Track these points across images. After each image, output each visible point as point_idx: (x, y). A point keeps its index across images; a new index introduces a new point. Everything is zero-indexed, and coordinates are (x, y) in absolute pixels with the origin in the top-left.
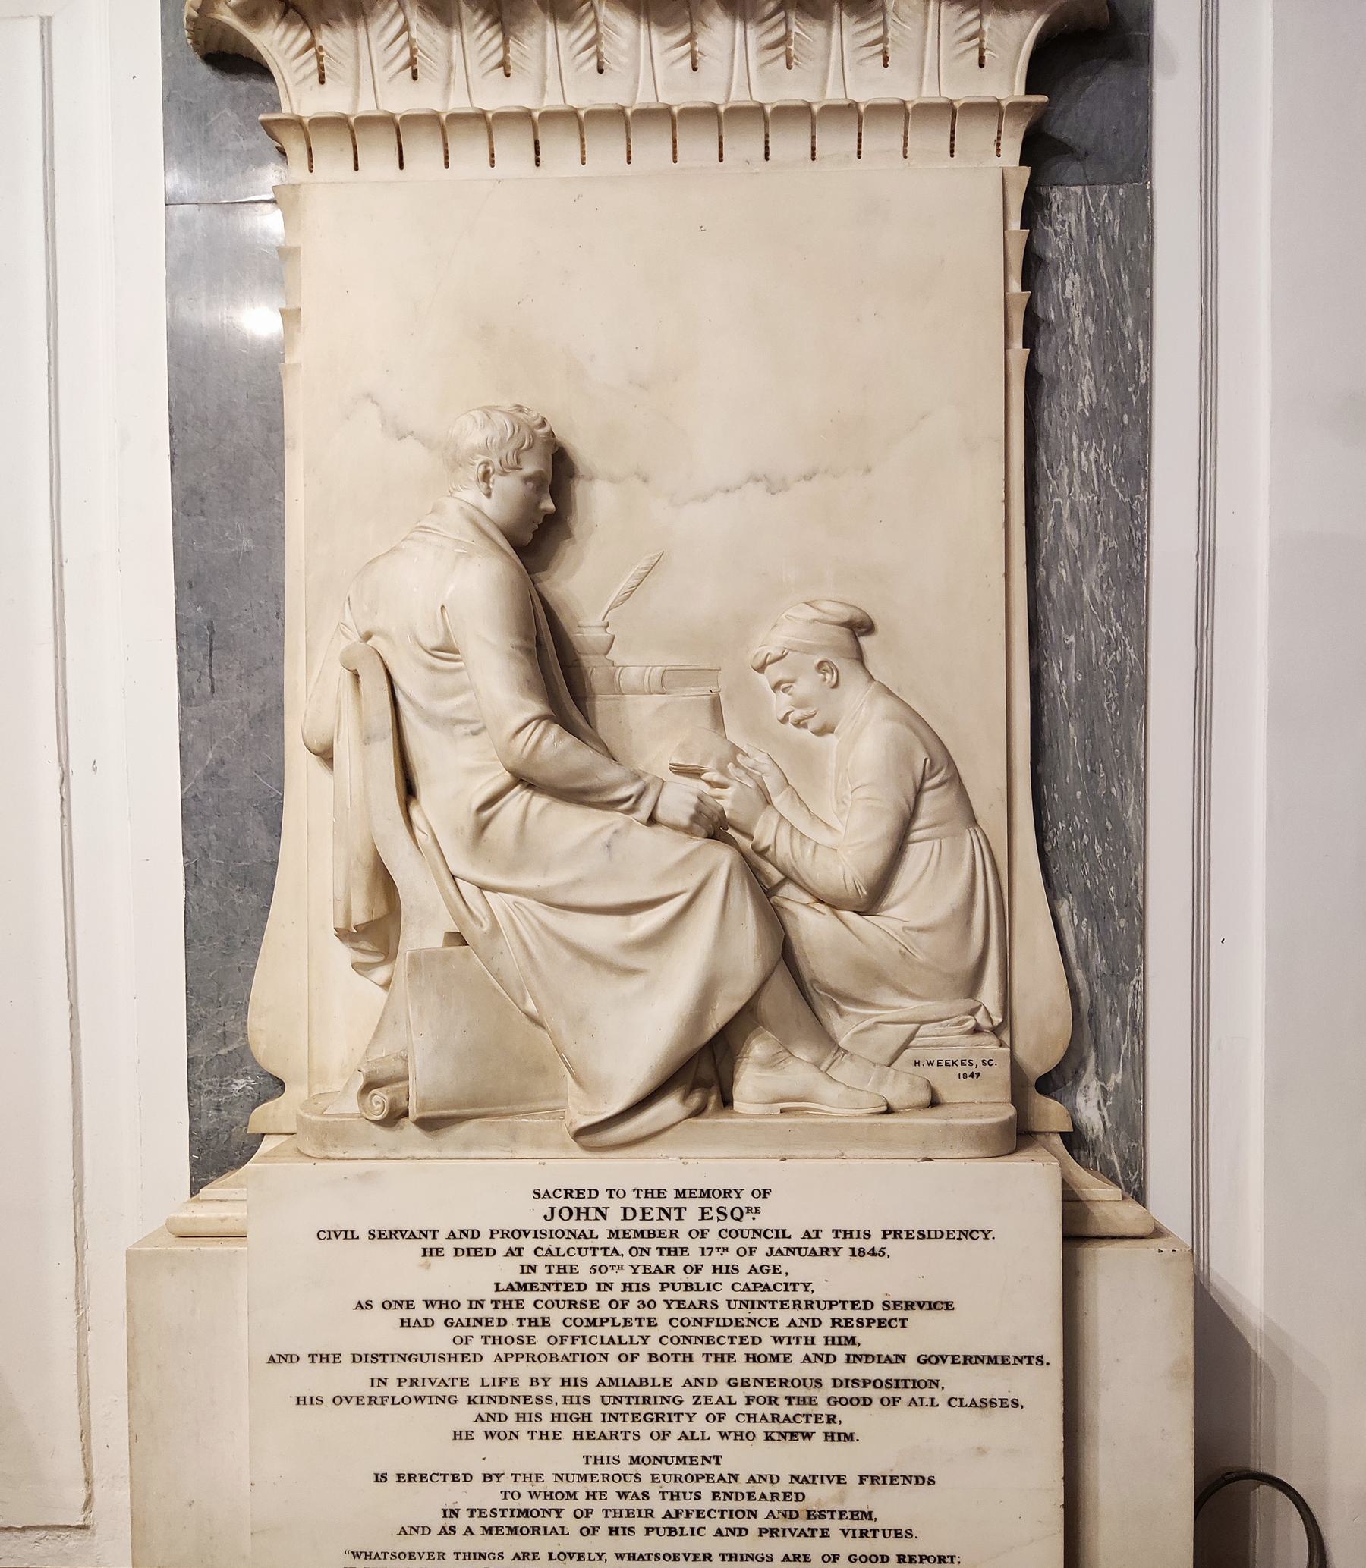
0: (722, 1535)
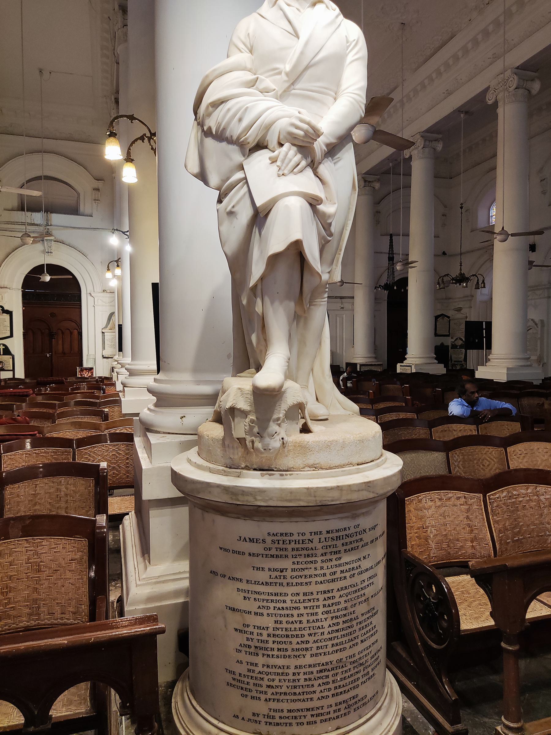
0: (299, 644)
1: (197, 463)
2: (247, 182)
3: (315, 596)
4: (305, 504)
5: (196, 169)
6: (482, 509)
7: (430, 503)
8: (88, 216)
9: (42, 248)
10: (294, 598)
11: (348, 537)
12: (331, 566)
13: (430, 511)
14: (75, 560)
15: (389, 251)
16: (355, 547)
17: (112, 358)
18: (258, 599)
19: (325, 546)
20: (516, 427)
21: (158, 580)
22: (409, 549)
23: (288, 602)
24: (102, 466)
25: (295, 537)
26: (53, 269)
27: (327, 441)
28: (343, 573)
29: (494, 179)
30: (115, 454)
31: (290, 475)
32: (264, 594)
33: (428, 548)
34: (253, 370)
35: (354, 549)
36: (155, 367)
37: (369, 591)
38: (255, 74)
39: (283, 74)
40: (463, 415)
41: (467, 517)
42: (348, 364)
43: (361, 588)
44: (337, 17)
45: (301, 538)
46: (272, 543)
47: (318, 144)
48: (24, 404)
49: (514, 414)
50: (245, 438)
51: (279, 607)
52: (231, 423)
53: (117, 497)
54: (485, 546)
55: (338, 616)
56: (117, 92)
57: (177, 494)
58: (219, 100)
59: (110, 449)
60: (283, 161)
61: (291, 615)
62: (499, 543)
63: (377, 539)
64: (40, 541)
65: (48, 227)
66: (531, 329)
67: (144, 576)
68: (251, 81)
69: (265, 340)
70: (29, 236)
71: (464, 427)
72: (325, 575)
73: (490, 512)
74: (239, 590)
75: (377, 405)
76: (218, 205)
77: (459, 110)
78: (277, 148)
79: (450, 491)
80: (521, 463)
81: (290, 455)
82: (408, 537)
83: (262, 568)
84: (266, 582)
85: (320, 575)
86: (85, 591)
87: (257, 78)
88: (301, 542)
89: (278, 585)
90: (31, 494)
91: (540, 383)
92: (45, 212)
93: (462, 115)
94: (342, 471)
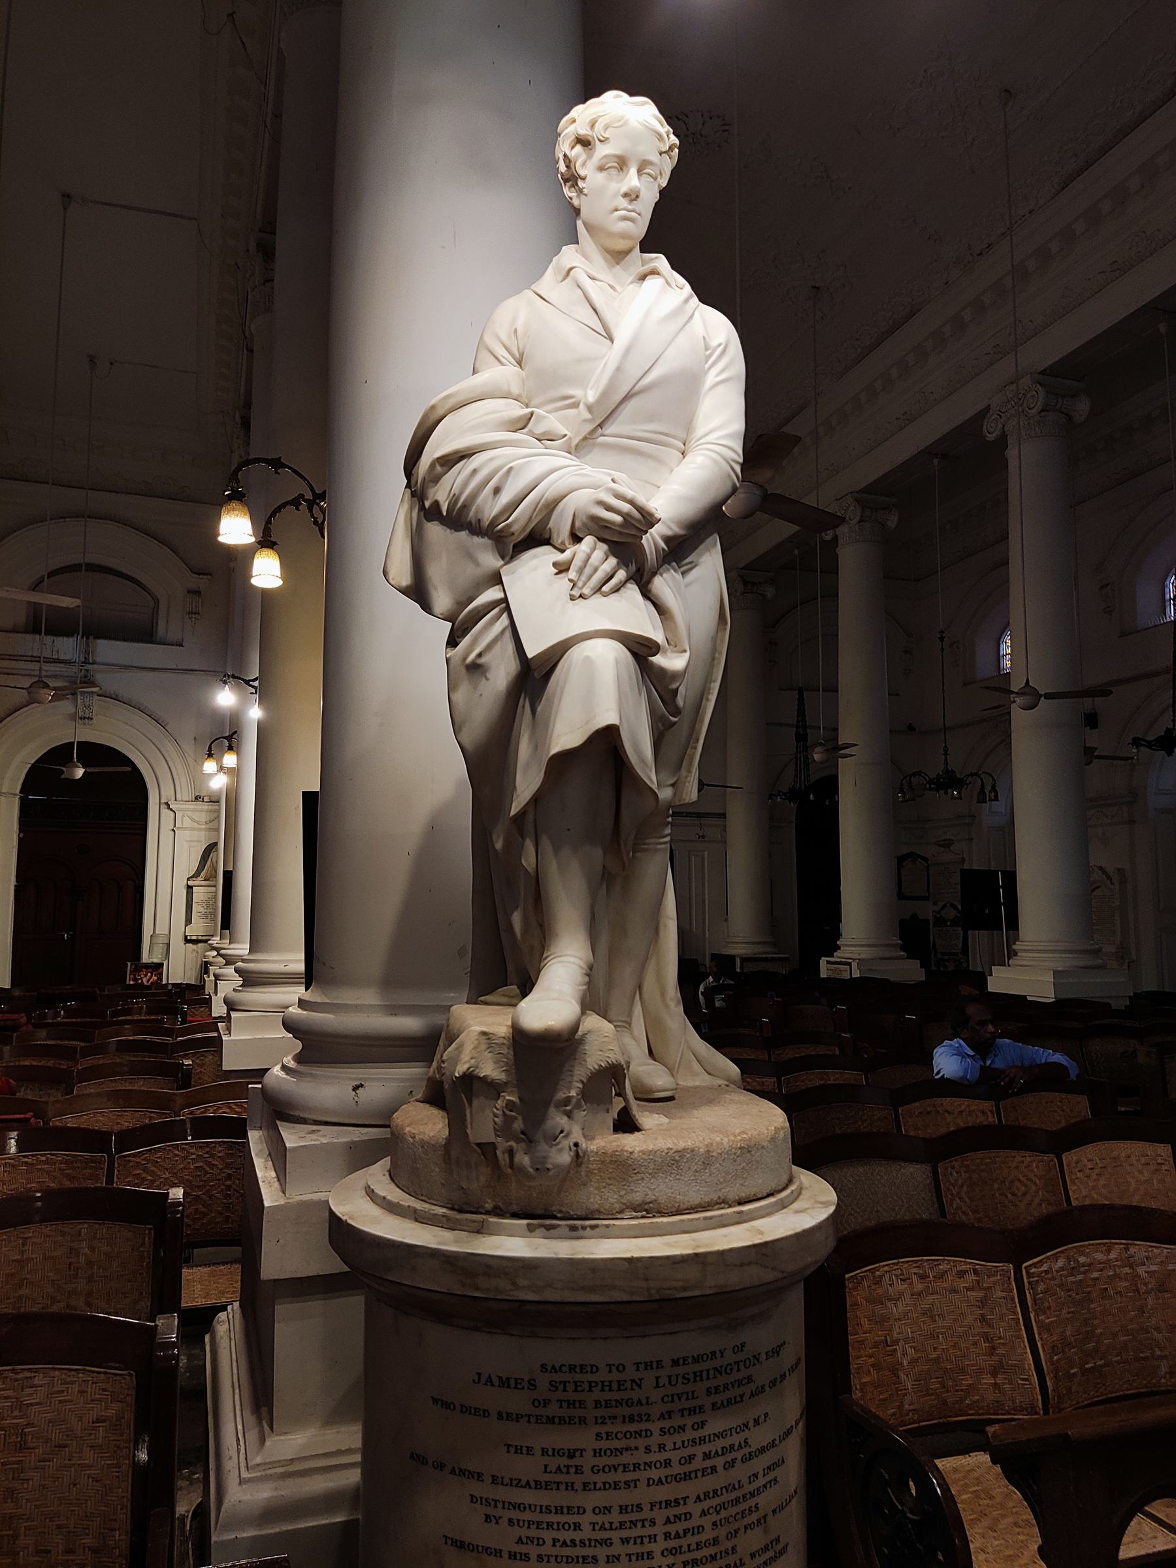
1: (388, 1198)
2: (508, 609)
3: (646, 1514)
4: (626, 1298)
5: (406, 580)
6: (1013, 1299)
7: (901, 1286)
8: (173, 645)
9: (73, 710)
10: (600, 1519)
11: (721, 1374)
12: (683, 1442)
13: (899, 1303)
14: (104, 1421)
15: (798, 722)
16: (735, 1397)
17: (206, 941)
18: (518, 1520)
19: (668, 1396)
20: (1079, 1107)
21: (291, 1469)
22: (857, 1395)
23: (587, 1529)
24: (173, 1197)
25: (602, 1375)
26: (93, 753)
27: (671, 1149)
28: (710, 1458)
29: (1003, 587)
30: (201, 1167)
31: (593, 1227)
32: (530, 1508)
33: (897, 1390)
34: (514, 989)
35: (733, 1402)
36: (301, 967)
37: (766, 1500)
38: (527, 406)
39: (582, 406)
40: (964, 1077)
41: (983, 1318)
42: (714, 957)
43: (750, 1492)
44: (686, 301)
45: (615, 1376)
46: (550, 1390)
47: (650, 538)
48: (6, 1049)
49: (1073, 1076)
50: (494, 1143)
51: (565, 1540)
52: (465, 1110)
53: (200, 1266)
54: (1022, 1384)
55: (697, 1559)
56: (248, 405)
57: (338, 1266)
58: (456, 452)
59: (192, 1154)
60: (581, 571)
61: (592, 1558)
62: (1052, 1375)
63: (783, 1376)
64: (28, 1374)
65: (89, 667)
66: (1099, 887)
67: (258, 1460)
68: (519, 419)
69: (541, 926)
70: (47, 686)
71: (968, 1106)
72: (668, 1463)
73: (1030, 1305)
74: (474, 1500)
75: (780, 1052)
76: (448, 650)
77: (929, 452)
78: (569, 544)
79: (942, 1258)
80: (1093, 1188)
81: (591, 1181)
82: (853, 1366)
83: (528, 1447)
84: (536, 1482)
85: (658, 1465)
86: (123, 1497)
87: (532, 414)
88: (615, 1386)
89: (563, 1487)
90: (13, 1261)
91: (1126, 1006)
92: (83, 637)
93: (935, 461)
94: (705, 1218)
